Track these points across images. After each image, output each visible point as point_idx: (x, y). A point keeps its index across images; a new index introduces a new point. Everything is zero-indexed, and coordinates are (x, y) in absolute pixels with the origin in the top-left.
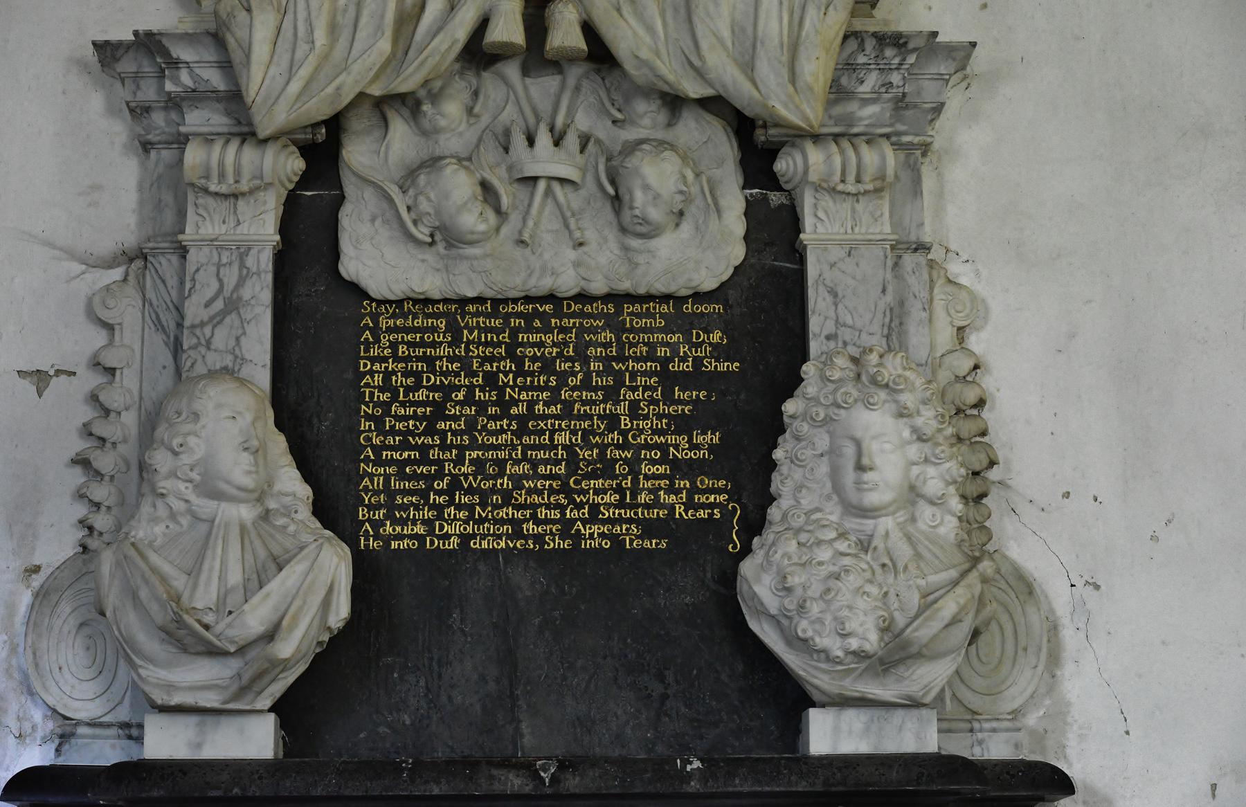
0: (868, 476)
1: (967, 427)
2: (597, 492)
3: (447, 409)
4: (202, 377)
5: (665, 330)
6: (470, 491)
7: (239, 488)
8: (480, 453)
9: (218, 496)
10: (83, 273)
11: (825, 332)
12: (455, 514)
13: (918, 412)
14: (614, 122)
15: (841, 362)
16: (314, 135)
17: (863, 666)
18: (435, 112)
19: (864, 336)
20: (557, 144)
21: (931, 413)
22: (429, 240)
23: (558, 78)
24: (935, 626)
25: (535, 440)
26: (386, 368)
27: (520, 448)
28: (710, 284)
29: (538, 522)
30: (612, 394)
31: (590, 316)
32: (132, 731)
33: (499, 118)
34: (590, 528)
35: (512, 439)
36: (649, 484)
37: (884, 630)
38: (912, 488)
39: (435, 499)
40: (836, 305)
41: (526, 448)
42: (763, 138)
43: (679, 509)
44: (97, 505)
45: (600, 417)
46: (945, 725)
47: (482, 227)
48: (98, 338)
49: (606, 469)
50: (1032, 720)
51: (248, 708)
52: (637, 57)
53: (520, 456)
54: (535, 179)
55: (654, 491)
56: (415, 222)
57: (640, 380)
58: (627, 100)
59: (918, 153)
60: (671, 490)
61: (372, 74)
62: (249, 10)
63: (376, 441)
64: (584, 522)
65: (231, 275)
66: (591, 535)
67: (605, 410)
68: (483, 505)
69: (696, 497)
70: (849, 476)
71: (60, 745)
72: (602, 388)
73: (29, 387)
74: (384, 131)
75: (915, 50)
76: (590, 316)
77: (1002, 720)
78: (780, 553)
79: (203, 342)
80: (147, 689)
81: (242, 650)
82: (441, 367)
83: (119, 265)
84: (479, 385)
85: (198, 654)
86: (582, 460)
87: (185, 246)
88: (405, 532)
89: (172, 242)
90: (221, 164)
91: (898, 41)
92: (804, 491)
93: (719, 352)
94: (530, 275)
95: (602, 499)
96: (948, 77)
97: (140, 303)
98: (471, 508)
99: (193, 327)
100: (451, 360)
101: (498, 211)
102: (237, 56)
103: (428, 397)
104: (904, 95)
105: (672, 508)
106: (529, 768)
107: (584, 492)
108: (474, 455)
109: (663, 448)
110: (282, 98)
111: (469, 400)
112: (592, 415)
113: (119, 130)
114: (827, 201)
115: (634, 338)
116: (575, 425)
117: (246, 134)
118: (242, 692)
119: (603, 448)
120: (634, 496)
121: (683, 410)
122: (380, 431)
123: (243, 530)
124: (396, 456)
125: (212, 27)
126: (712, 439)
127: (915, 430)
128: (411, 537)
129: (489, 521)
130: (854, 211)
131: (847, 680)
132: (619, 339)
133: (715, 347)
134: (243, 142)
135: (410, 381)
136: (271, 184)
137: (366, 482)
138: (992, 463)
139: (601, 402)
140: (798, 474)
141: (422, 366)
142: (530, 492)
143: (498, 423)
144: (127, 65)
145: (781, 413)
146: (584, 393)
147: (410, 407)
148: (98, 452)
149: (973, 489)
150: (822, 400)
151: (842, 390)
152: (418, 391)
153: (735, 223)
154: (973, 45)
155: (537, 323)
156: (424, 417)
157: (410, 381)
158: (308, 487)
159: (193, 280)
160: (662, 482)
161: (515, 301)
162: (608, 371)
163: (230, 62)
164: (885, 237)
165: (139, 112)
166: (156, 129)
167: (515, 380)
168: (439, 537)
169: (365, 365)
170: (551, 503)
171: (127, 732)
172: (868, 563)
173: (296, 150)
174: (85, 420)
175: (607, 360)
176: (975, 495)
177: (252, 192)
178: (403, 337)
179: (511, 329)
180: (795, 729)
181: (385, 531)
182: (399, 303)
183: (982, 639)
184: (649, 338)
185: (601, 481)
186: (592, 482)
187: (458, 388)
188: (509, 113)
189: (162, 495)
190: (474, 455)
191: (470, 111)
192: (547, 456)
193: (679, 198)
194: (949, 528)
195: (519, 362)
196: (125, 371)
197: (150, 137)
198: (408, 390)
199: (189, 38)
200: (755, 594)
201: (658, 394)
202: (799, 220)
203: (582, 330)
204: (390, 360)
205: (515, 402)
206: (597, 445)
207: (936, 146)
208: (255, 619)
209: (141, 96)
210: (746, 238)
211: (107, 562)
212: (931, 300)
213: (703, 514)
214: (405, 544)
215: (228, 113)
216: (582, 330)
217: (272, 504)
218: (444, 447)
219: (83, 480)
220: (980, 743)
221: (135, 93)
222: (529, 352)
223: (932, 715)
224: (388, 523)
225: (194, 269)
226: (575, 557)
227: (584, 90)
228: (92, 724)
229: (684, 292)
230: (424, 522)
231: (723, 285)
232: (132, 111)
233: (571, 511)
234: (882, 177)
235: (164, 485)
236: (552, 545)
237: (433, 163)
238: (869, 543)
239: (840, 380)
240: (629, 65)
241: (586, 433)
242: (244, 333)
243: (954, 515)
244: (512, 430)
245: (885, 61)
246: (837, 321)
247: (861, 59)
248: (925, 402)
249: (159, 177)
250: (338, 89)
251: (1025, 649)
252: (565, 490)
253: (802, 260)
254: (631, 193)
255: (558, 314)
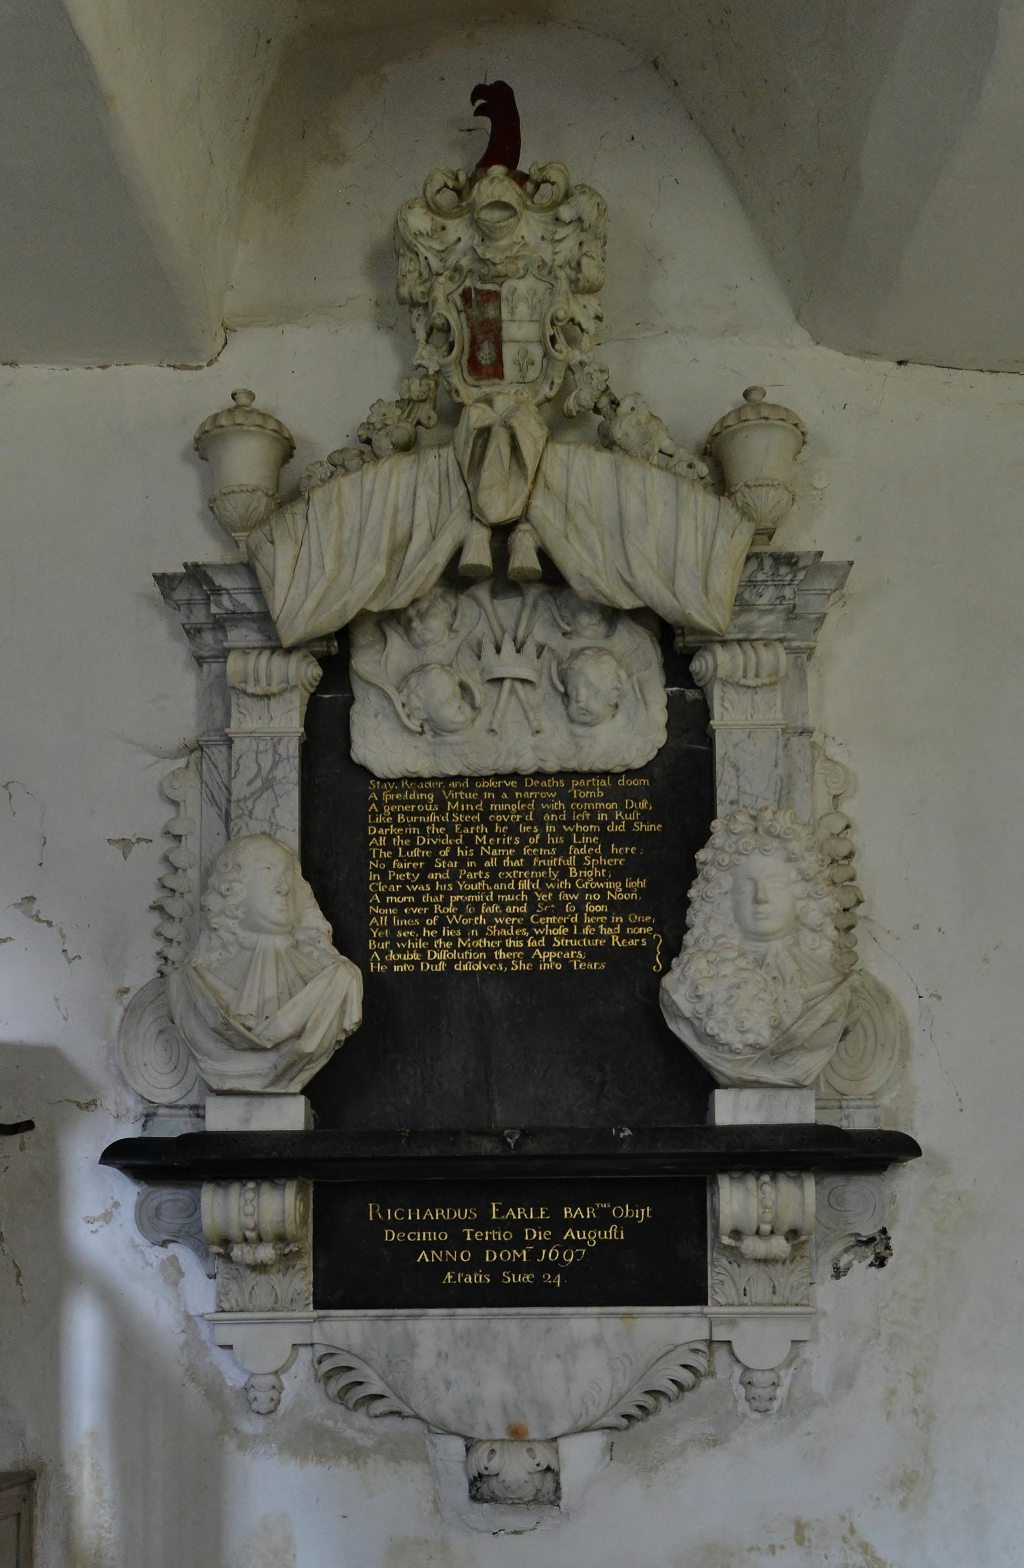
0: (761, 908)
1: (840, 874)
2: (551, 926)
3: (435, 863)
4: (245, 837)
5: (603, 800)
6: (454, 927)
7: (275, 924)
8: (461, 897)
9: (257, 929)
10: (156, 763)
11: (730, 798)
12: (442, 945)
13: (803, 859)
14: (564, 634)
15: (742, 818)
16: (329, 647)
17: (759, 1055)
18: (422, 627)
19: (759, 801)
20: (518, 651)
21: (814, 858)
22: (420, 730)
23: (519, 599)
24: (816, 1024)
25: (503, 887)
26: (389, 832)
27: (492, 893)
28: (638, 763)
29: (506, 950)
30: (562, 851)
31: (545, 789)
32: (198, 1111)
33: (475, 631)
34: (546, 954)
35: (486, 887)
36: (591, 920)
37: (775, 1028)
38: (797, 918)
39: (427, 934)
40: (738, 777)
41: (496, 893)
42: (681, 645)
43: (615, 939)
44: (170, 941)
45: (554, 868)
46: (820, 1103)
47: (461, 718)
48: (168, 812)
49: (558, 908)
50: (886, 1101)
51: (283, 1091)
52: (581, 575)
53: (492, 899)
54: (500, 680)
55: (595, 925)
56: (409, 716)
57: (585, 839)
58: (574, 615)
59: (805, 656)
60: (609, 924)
61: (371, 593)
62: (272, 543)
63: (381, 889)
64: (542, 950)
65: (266, 762)
66: (547, 960)
67: (557, 862)
68: (464, 937)
69: (628, 929)
70: (748, 908)
71: (146, 1122)
72: (555, 846)
73: (116, 851)
74: (383, 644)
75: (804, 568)
76: (545, 789)
77: (865, 1099)
78: (693, 968)
79: (246, 812)
80: (205, 1078)
81: (276, 1047)
82: (430, 831)
83: (183, 756)
84: (460, 845)
85: (245, 1050)
86: (539, 902)
87: (231, 738)
88: (404, 958)
89: (222, 736)
90: (256, 671)
91: (790, 560)
92: (712, 921)
93: (646, 817)
94: (499, 757)
95: (556, 931)
96: (829, 592)
97: (199, 785)
98: (454, 939)
99: (239, 801)
100: (438, 825)
101: (474, 707)
102: (264, 582)
103: (420, 854)
104: (794, 607)
105: (609, 938)
106: (499, 1136)
107: (542, 927)
108: (457, 898)
109: (603, 892)
110: (301, 613)
111: (453, 856)
112: (548, 867)
113: (180, 650)
114: (731, 693)
115: (580, 806)
116: (534, 874)
117: (276, 647)
118: (278, 1079)
119: (556, 892)
120: (580, 929)
121: (618, 862)
122: (385, 881)
123: (278, 955)
124: (397, 900)
125: (245, 560)
126: (640, 884)
127: (800, 872)
128: (409, 962)
129: (468, 949)
130: (753, 700)
131: (746, 1067)
132: (568, 808)
133: (643, 812)
134: (272, 653)
135: (407, 842)
136: (296, 686)
137: (374, 920)
138: (859, 902)
139: (554, 856)
140: (707, 908)
141: (416, 831)
142: (500, 927)
143: (475, 874)
144: (181, 594)
145: (694, 861)
146: (541, 850)
147: (407, 862)
148: (170, 900)
149: (845, 921)
150: (727, 849)
151: (744, 840)
152: (413, 850)
153: (660, 715)
154: (851, 563)
155: (505, 796)
156: (417, 870)
157: (407, 842)
158: (329, 923)
159: (238, 764)
160: (602, 918)
161: (487, 778)
162: (560, 832)
163: (260, 588)
164: (778, 722)
165: (193, 632)
166: (207, 646)
167: (487, 840)
168: (431, 962)
169: (372, 830)
170: (516, 935)
171: (196, 1112)
172: (762, 976)
173: (314, 659)
174: (160, 876)
175: (558, 824)
176: (846, 926)
177: (281, 693)
178: (401, 808)
179: (484, 801)
180: (704, 1105)
181: (389, 957)
182: (398, 781)
183: (849, 1037)
184: (591, 806)
185: (554, 918)
186: (548, 918)
187: (444, 847)
188: (482, 627)
189: (215, 929)
190: (457, 898)
191: (450, 627)
192: (513, 899)
193: (615, 693)
194: (825, 950)
195: (491, 826)
196: (189, 837)
197: (203, 653)
198: (406, 849)
199: (228, 568)
200: (673, 1002)
201: (599, 850)
202: (709, 711)
203: (539, 801)
204: (392, 826)
205: (488, 858)
206: (551, 890)
207: (818, 652)
208: (286, 1023)
209: (194, 619)
210: (668, 726)
211: (174, 980)
212: (813, 775)
213: (633, 943)
214: (404, 968)
215: (261, 631)
216: (539, 801)
217: (301, 936)
218: (434, 893)
219: (158, 922)
220: (847, 1117)
221: (188, 617)
222: (499, 818)
223: (810, 1095)
224: (392, 952)
225: (237, 756)
226: (535, 976)
227: (540, 609)
228: (170, 1106)
229: (618, 770)
230: (419, 951)
231: (649, 763)
232: (188, 632)
233: (531, 941)
234: (776, 673)
235: (216, 921)
236: (517, 967)
237: (422, 669)
238: (763, 961)
239: (741, 833)
240: (574, 582)
241: (543, 881)
242: (278, 806)
243: (829, 939)
244: (485, 879)
245: (779, 578)
246: (739, 789)
247: (761, 577)
248: (809, 849)
249: (210, 685)
250: (344, 605)
251: (883, 1046)
252: (527, 925)
253: (711, 742)
254: (577, 690)
255: (521, 788)
